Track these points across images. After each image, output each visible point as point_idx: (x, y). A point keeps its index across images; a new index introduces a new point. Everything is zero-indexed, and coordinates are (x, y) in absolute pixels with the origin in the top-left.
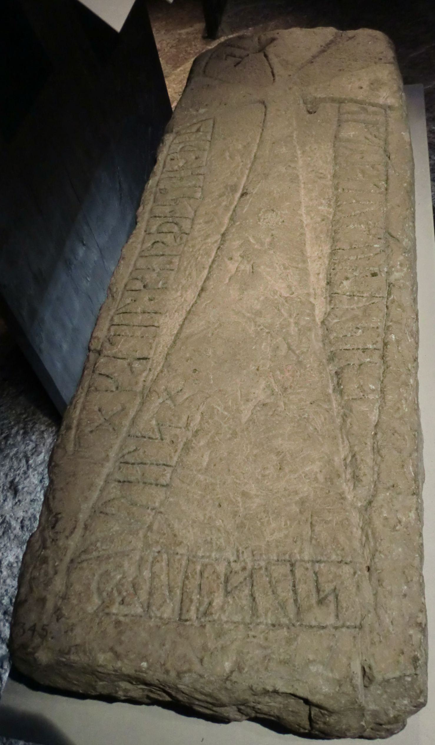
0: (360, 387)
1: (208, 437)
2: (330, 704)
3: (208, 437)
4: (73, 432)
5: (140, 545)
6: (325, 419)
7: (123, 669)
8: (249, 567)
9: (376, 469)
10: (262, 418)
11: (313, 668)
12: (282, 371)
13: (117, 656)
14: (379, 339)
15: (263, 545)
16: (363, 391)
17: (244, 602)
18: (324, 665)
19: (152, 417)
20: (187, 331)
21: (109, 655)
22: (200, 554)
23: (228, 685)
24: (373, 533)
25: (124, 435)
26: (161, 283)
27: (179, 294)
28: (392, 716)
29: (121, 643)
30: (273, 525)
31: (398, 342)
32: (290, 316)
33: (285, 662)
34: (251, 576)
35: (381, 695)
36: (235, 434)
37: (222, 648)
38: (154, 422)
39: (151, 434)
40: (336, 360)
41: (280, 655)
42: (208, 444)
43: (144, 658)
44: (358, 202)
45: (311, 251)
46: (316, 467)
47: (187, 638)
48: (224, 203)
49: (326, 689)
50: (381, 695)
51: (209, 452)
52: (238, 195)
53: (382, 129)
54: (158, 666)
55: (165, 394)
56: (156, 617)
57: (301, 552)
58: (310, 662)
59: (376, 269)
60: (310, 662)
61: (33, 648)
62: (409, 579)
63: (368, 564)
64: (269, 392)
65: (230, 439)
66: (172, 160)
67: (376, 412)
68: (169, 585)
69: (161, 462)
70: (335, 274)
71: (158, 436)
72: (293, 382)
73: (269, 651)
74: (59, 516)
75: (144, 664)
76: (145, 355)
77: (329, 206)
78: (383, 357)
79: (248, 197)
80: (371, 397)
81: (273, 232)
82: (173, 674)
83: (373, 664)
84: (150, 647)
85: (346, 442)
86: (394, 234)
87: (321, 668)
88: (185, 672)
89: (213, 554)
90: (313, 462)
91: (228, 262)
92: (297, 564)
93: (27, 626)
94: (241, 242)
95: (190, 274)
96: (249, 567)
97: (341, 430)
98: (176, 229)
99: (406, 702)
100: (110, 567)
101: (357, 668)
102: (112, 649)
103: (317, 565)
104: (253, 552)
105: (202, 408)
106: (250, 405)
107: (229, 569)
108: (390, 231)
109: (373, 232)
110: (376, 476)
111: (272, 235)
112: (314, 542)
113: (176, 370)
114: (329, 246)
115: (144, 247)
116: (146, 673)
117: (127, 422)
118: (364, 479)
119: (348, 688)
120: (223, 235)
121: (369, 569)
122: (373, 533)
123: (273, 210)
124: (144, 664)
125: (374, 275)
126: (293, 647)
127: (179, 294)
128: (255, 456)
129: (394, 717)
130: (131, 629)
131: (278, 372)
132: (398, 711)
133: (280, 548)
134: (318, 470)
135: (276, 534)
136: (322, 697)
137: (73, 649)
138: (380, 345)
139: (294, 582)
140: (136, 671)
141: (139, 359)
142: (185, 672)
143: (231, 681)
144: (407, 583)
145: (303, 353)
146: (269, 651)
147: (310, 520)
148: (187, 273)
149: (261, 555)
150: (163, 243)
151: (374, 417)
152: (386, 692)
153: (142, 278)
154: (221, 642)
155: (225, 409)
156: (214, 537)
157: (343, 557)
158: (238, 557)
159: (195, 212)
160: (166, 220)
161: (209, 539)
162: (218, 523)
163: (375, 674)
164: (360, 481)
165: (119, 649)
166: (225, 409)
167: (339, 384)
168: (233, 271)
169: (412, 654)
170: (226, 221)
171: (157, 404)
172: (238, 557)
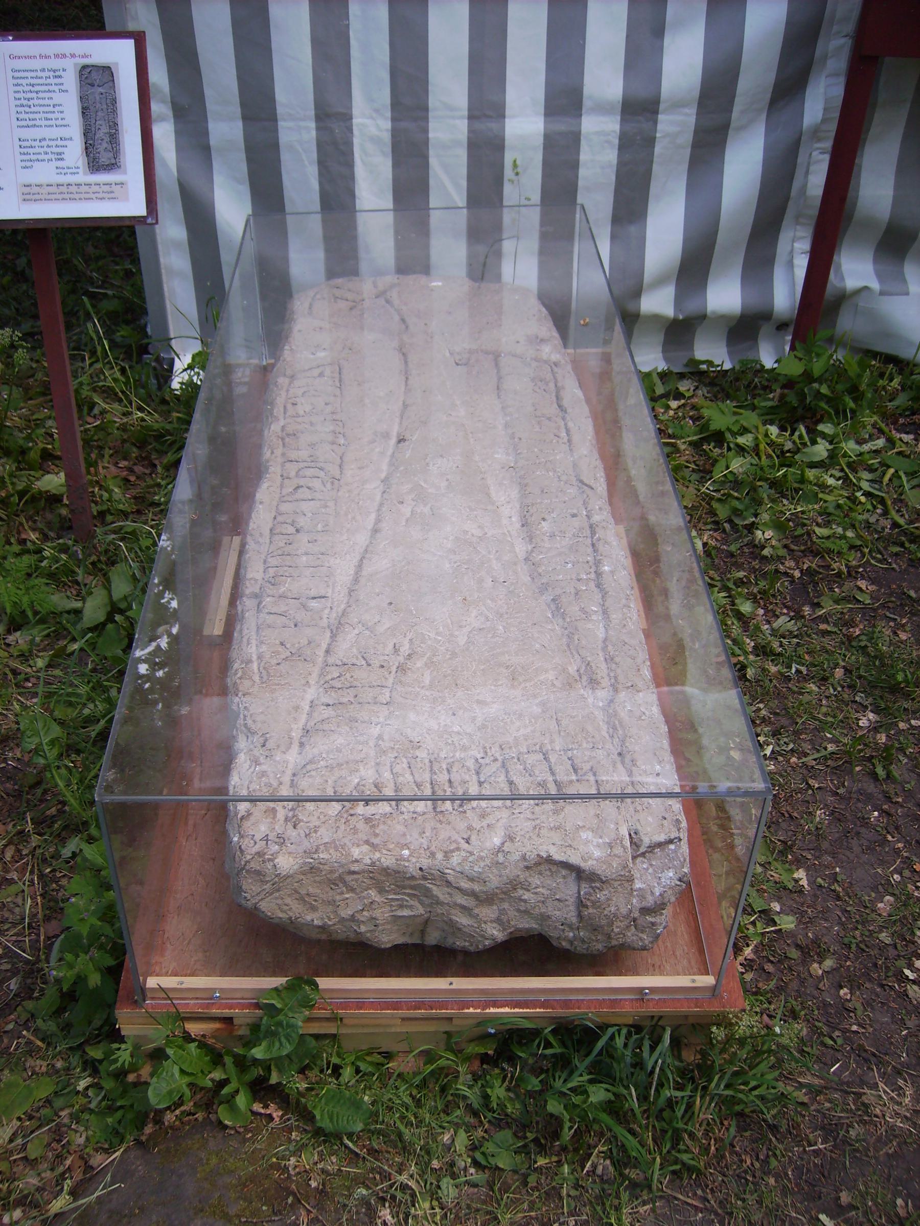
0: (582, 610)
1: (425, 659)
2: (601, 870)
3: (425, 659)
4: (255, 666)
5: (372, 753)
6: (551, 637)
7: (383, 860)
8: (500, 758)
9: (612, 674)
10: (482, 640)
11: (584, 835)
12: (493, 600)
13: (374, 847)
14: (592, 570)
15: (511, 740)
16: (585, 613)
17: (502, 785)
18: (593, 831)
19: (352, 646)
20: (367, 570)
21: (366, 848)
22: (443, 755)
23: (501, 858)
24: (620, 723)
25: (321, 665)
26: (320, 525)
27: (345, 537)
28: (658, 894)
29: (376, 835)
30: (518, 724)
31: (612, 572)
32: (489, 552)
33: (557, 828)
34: (504, 765)
35: (647, 869)
36: (454, 655)
37: (488, 826)
38: (355, 650)
39: (355, 661)
40: (550, 589)
41: (549, 823)
42: (426, 664)
43: (406, 846)
44: (541, 450)
45: (499, 496)
46: (551, 676)
47: (449, 823)
48: (377, 450)
49: (597, 853)
50: (647, 869)
51: (429, 671)
52: (394, 441)
53: (552, 385)
54: (422, 851)
55: (360, 625)
56: (409, 812)
57: (552, 741)
58: (579, 828)
59: (575, 511)
60: (579, 828)
61: (272, 855)
62: (661, 759)
63: (619, 750)
64: (483, 619)
65: (450, 659)
66: (294, 404)
67: (602, 630)
68: (415, 782)
69: (375, 684)
70: (531, 516)
71: (364, 662)
72: (508, 608)
73: (538, 822)
74: (268, 736)
75: (406, 852)
76: (322, 593)
77: (508, 454)
78: (598, 586)
79: (407, 443)
80: (594, 617)
81: (449, 477)
82: (440, 856)
83: (639, 828)
84: (408, 837)
85: (577, 656)
86: (586, 481)
87: (590, 834)
88: (453, 851)
89: (457, 755)
90: (546, 671)
91: (400, 506)
92: (550, 752)
93: (258, 837)
94: (410, 486)
95: (354, 518)
96: (500, 758)
97: (569, 646)
98: (322, 474)
99: (671, 874)
100: (344, 773)
101: (624, 832)
102: (367, 842)
103: (570, 752)
104: (501, 746)
105: (409, 636)
106: (466, 630)
107: (478, 765)
108: (582, 478)
109: (564, 478)
110: (613, 681)
111: (447, 480)
112: (562, 734)
113: (367, 604)
114: (516, 491)
115: (285, 492)
116: (408, 861)
117: (321, 653)
118: (602, 681)
119: (618, 850)
120: (385, 481)
121: (620, 754)
122: (620, 723)
123: (441, 456)
124: (406, 852)
125: (574, 516)
126: (561, 816)
127: (345, 537)
128: (483, 670)
129: (661, 895)
130: (384, 823)
131: (489, 602)
132: (664, 887)
133: (530, 741)
134: (554, 678)
135: (522, 730)
136: (595, 862)
137: (322, 847)
138: (593, 576)
139: (550, 766)
140: (397, 860)
141: (314, 598)
142: (453, 851)
143: (503, 851)
144: (660, 762)
145: (512, 584)
146: (538, 822)
147: (555, 717)
148: (350, 517)
149: (510, 748)
150: (309, 488)
151: (601, 634)
152: (651, 865)
153: (293, 521)
154: (485, 823)
155: (437, 634)
156: (455, 740)
157: (594, 743)
158: (486, 753)
159: (341, 458)
160: (306, 464)
161: (450, 741)
162: (456, 728)
163: (643, 838)
164: (598, 683)
165: (376, 841)
166: (437, 634)
167: (558, 608)
168: (408, 515)
169: (675, 818)
170: (385, 467)
171: (353, 635)
172: (486, 753)
